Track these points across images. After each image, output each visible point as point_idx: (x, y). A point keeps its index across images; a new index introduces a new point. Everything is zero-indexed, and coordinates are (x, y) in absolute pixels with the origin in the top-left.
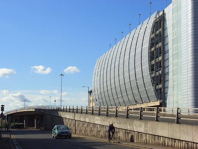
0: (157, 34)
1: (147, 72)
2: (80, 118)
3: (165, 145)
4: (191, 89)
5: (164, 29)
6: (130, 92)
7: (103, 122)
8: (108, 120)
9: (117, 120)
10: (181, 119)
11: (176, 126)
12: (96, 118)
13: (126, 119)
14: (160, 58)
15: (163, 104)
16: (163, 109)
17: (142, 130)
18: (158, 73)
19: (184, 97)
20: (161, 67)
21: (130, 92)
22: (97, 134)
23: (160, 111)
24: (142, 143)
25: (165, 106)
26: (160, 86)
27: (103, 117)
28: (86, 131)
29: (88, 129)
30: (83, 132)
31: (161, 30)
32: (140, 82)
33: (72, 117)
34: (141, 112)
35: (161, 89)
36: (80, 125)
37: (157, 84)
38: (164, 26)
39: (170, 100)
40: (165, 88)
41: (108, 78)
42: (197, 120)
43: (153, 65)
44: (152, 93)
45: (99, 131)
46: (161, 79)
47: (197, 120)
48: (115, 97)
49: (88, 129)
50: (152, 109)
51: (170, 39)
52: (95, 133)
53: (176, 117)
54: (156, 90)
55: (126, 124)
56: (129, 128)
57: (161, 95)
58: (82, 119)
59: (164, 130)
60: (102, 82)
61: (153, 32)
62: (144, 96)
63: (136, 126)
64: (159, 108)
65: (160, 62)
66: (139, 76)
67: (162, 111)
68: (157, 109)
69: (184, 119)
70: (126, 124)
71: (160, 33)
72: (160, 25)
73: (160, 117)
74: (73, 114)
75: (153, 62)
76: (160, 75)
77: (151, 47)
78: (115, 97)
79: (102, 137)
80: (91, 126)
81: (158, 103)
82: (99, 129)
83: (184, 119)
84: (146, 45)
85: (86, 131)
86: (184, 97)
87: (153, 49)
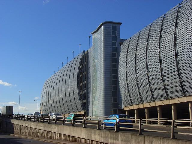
0: (84, 66)
1: (76, 91)
2: (23, 123)
3: (66, 140)
4: (103, 103)
5: (88, 63)
6: (65, 105)
7: (36, 126)
8: (39, 125)
9: (43, 124)
10: (179, 133)
11: (72, 127)
12: (52, 126)
13: (48, 124)
14: (85, 82)
15: (86, 113)
16: (137, 120)
17: (55, 131)
18: (83, 92)
19: (99, 108)
20: (85, 88)
21: (65, 105)
22: (32, 135)
23: (143, 123)
24: (55, 140)
25: (88, 115)
26: (85, 101)
27: (36, 123)
28: (26, 133)
29: (28, 132)
30: (24, 133)
31: (86, 63)
32: (72, 98)
33: (18, 123)
34: (141, 125)
35: (85, 103)
36: (15, 125)
37: (83, 100)
38: (88, 61)
39: (90, 110)
40: (88, 102)
41: (54, 93)
42: (191, 134)
43: (81, 87)
44: (79, 106)
45: (34, 132)
46: (85, 96)
47: (191, 134)
48: (56, 108)
49: (28, 132)
50: (151, 121)
51: (91, 69)
52: (31, 134)
53: (115, 126)
54: (82, 104)
55: (48, 127)
56: (49, 130)
57: (85, 106)
58: (24, 125)
59: (82, 133)
60: (47, 97)
61: (81, 64)
62: (74, 107)
63: (53, 129)
64: (143, 120)
65: (85, 84)
66: (71, 94)
67: (146, 123)
68: (141, 121)
69: (186, 134)
70: (48, 127)
71: (85, 65)
72: (85, 60)
73: (179, 133)
74: (19, 121)
75: (81, 84)
76: (85, 93)
77: (79, 75)
78: (56, 108)
79: (35, 137)
80: (29, 129)
81: (83, 113)
82: (34, 131)
83: (186, 134)
84: (76, 73)
85: (29, 132)
86: (99, 108)
87: (81, 76)
